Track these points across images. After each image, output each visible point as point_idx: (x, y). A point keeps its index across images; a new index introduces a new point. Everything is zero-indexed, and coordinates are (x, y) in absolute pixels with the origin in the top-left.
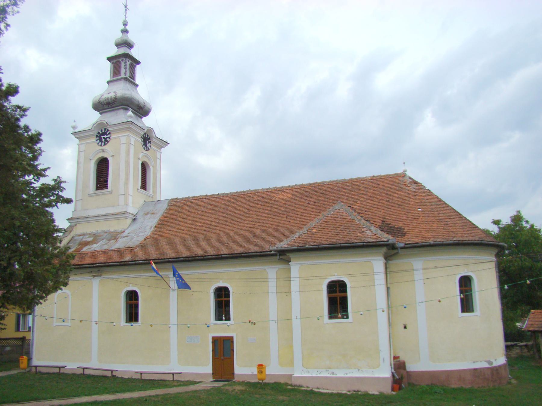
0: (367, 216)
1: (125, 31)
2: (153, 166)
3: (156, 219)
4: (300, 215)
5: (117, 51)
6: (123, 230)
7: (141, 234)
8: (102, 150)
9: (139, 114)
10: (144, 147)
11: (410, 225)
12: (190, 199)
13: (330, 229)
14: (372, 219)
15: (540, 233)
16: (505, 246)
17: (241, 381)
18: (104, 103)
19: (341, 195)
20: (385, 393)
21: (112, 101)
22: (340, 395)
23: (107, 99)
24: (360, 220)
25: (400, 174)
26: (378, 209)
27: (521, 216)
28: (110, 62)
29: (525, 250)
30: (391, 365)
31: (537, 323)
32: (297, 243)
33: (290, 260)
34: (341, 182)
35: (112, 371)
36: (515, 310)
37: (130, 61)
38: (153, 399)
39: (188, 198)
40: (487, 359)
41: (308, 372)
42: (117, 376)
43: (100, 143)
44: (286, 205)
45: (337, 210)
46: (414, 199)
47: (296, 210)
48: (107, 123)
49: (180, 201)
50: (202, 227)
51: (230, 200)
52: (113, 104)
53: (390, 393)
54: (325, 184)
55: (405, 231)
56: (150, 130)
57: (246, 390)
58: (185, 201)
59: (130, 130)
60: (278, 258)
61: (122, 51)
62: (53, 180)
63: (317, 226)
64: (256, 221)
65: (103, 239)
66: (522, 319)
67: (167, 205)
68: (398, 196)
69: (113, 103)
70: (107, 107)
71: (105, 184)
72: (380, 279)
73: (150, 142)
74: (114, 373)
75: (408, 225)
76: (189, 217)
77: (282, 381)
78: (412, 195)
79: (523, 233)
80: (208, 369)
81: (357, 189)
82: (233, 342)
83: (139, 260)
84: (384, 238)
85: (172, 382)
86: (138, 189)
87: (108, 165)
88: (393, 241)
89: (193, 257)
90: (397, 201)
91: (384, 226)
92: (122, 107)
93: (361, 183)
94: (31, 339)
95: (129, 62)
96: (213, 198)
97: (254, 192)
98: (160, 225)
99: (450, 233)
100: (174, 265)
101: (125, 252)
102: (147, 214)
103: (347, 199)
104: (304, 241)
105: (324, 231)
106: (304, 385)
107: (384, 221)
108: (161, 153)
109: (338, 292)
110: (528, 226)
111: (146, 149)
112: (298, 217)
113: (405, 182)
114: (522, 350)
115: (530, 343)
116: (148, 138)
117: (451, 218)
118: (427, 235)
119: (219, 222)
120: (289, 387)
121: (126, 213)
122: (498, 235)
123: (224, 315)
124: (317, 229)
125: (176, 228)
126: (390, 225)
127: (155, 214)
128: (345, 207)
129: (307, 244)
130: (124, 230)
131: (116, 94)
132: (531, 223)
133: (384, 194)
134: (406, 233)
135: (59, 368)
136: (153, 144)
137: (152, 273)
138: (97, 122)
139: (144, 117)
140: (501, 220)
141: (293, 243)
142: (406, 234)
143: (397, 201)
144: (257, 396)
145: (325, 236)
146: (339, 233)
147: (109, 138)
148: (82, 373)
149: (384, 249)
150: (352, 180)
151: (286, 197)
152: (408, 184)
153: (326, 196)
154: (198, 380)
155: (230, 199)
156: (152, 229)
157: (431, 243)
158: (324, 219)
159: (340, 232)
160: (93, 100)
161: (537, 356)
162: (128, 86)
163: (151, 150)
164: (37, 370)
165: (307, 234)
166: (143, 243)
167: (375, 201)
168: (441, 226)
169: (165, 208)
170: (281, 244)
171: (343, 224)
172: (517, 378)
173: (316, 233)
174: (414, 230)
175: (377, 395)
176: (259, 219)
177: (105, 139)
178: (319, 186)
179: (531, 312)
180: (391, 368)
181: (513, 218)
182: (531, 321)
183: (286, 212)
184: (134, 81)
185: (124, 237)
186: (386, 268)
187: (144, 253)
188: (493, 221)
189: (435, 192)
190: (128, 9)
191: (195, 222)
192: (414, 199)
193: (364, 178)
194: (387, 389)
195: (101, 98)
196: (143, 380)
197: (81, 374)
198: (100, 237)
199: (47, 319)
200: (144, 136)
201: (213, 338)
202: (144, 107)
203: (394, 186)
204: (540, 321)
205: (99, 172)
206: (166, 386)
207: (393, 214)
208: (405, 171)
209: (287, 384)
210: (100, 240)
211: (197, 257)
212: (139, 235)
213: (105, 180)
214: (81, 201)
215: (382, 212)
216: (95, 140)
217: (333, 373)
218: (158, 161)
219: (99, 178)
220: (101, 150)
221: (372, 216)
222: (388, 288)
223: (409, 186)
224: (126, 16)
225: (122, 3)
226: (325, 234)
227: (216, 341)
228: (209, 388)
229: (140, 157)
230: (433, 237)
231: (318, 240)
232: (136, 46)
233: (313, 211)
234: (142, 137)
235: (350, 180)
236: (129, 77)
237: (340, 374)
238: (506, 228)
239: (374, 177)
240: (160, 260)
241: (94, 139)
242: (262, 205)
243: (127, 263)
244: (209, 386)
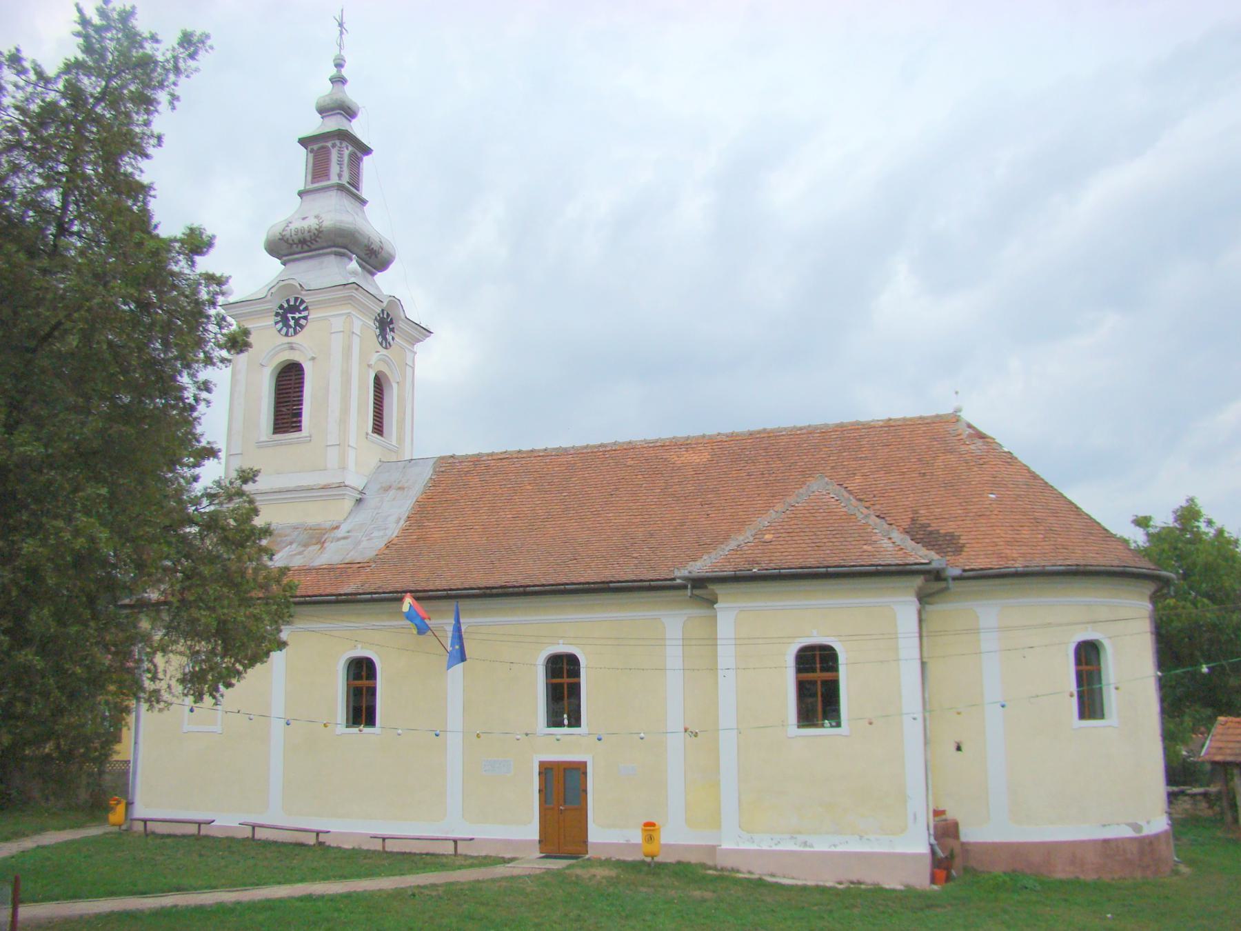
0: (878, 507)
1: (339, 80)
2: (398, 383)
3: (409, 502)
4: (731, 501)
5: (322, 125)
6: (335, 524)
7: (376, 534)
8: (290, 345)
9: (369, 267)
10: (380, 340)
11: (971, 530)
12: (482, 459)
13: (802, 534)
14: (889, 515)
15: (1237, 547)
16: (1173, 579)
17: (603, 858)
19: (820, 459)
20: (918, 887)
21: (311, 237)
22: (822, 890)
24: (867, 516)
25: (948, 415)
26: (903, 493)
27: (1197, 509)
29: (1204, 585)
30: (928, 829)
31: (1231, 745)
32: (733, 564)
33: (717, 599)
34: (818, 431)
35: (318, 833)
36: (1178, 717)
37: (350, 148)
38: (426, 892)
39: (478, 455)
40: (1130, 821)
41: (752, 840)
42: (327, 844)
43: (285, 330)
44: (700, 478)
45: (817, 493)
46: (980, 472)
47: (721, 489)
48: (301, 286)
49: (462, 462)
50: (514, 522)
51: (574, 463)
52: (312, 243)
53: (928, 889)
54: (784, 433)
55: (961, 541)
56: (395, 302)
57: (618, 877)
58: (472, 463)
59: (352, 303)
60: (689, 594)
61: (333, 124)
63: (773, 528)
64: (634, 511)
65: (291, 543)
66: (1194, 736)
67: (431, 472)
68: (945, 465)
69: (313, 242)
70: (299, 249)
71: (295, 420)
72: (909, 647)
73: (392, 330)
74: (322, 838)
75: (969, 530)
76: (483, 499)
77: (693, 858)
78: (974, 463)
79: (1201, 547)
80: (532, 832)
81: (855, 447)
82: (585, 773)
83: (381, 591)
84: (921, 557)
85: (453, 857)
86: (367, 434)
87: (303, 378)
88: (940, 564)
89: (501, 587)
90: (941, 476)
91: (916, 529)
92: (334, 249)
93: (864, 434)
94: (132, 759)
95: (347, 149)
96: (535, 457)
97: (625, 447)
99: (1057, 548)
100: (460, 603)
101: (346, 572)
102: (388, 489)
103: (833, 468)
104: (748, 559)
105: (789, 538)
106: (744, 869)
107: (916, 519)
109: (818, 670)
110: (1212, 532)
112: (728, 504)
113: (958, 435)
114: (1196, 804)
115: (1213, 789)
116: (389, 320)
117: (1060, 515)
118: (1008, 551)
119: (552, 510)
120: (711, 872)
121: (343, 485)
122: (1146, 549)
123: (565, 716)
124: (773, 534)
125: (454, 522)
126: (929, 529)
127: (406, 489)
128: (834, 488)
129: (755, 565)
130: (338, 525)
131: (321, 221)
132: (1218, 523)
133: (915, 460)
134: (963, 546)
135: (197, 825)
138: (278, 283)
139: (379, 273)
140: (1153, 516)
141: (725, 564)
142: (966, 549)
143: (941, 476)
144: (644, 890)
145: (792, 549)
146: (823, 544)
147: (305, 318)
148: (250, 835)
149: (919, 581)
150: (842, 427)
151: (698, 460)
152: (966, 438)
153: (787, 461)
154: (508, 855)
155: (573, 462)
156: (402, 522)
157: (1019, 569)
158: (788, 512)
159: (825, 540)
161: (1229, 817)
162: (348, 203)
164: (148, 828)
165: (753, 544)
166: (384, 554)
167: (893, 474)
168: (1039, 532)
169: (428, 478)
170: (699, 564)
171: (830, 525)
172: (1191, 862)
173: (772, 543)
174: (980, 541)
175: (901, 891)
176: (640, 507)
177: (297, 321)
178: (769, 437)
179: (1217, 722)
180: (929, 834)
181: (1179, 513)
182: (1219, 741)
183: (699, 494)
184: (357, 192)
185: (339, 539)
186: (920, 621)
187: (389, 577)
188: (1135, 518)
189: (1023, 458)
190: (346, 30)
191: (498, 511)
192: (980, 472)
193: (868, 423)
194: (921, 879)
195: (287, 228)
196: (387, 852)
197: (248, 838)
198: (285, 538)
199: (251, 719)
200: (381, 315)
201: (542, 764)
202: (380, 250)
203: (935, 443)
204: (1238, 742)
205: (279, 394)
206: (444, 866)
207: (934, 503)
208: (958, 410)
209: (704, 866)
210: (284, 545)
211: (510, 587)
212: (372, 535)
213: (294, 411)
214: (240, 456)
215: (910, 499)
216: (273, 323)
217: (805, 844)
218: (409, 370)
219: (280, 407)
220: (286, 346)
221: (888, 508)
222: (923, 664)
223: (967, 443)
224: (340, 46)
225: (334, 17)
226: (794, 546)
227: (547, 770)
228: (538, 872)
229: (372, 362)
230: (1022, 555)
231: (778, 558)
232: (362, 113)
233: (759, 492)
234: (376, 319)
235: (837, 425)
236: (348, 182)
237: (821, 845)
238: (1163, 536)
239: (891, 422)
240: (426, 593)
241: (271, 320)
242: (646, 476)
243: (353, 597)
244: (537, 867)
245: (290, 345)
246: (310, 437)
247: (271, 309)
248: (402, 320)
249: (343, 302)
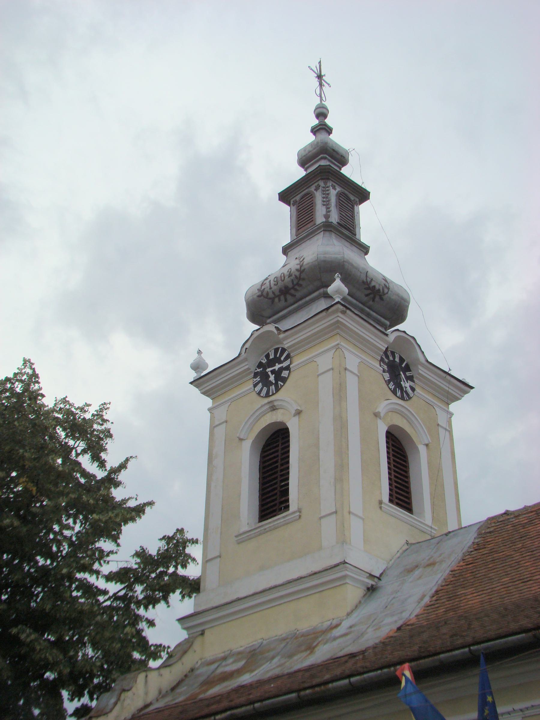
2: (427, 445)
6: (335, 622)
10: (392, 386)
18: (273, 293)
21: (292, 281)
23: (279, 279)
28: (289, 205)
37: (338, 189)
52: (296, 290)
58: (534, 513)
62: (164, 538)
69: (297, 287)
71: (283, 499)
86: (381, 502)
98: (450, 586)
108: (451, 414)
111: (399, 394)
136: (420, 383)
147: (288, 368)
163: (414, 399)
177: (277, 374)
198: (267, 654)
202: (386, 291)
224: (321, 96)
234: (382, 360)
245: (271, 405)
246: (300, 512)
247: (248, 369)
248: (422, 365)
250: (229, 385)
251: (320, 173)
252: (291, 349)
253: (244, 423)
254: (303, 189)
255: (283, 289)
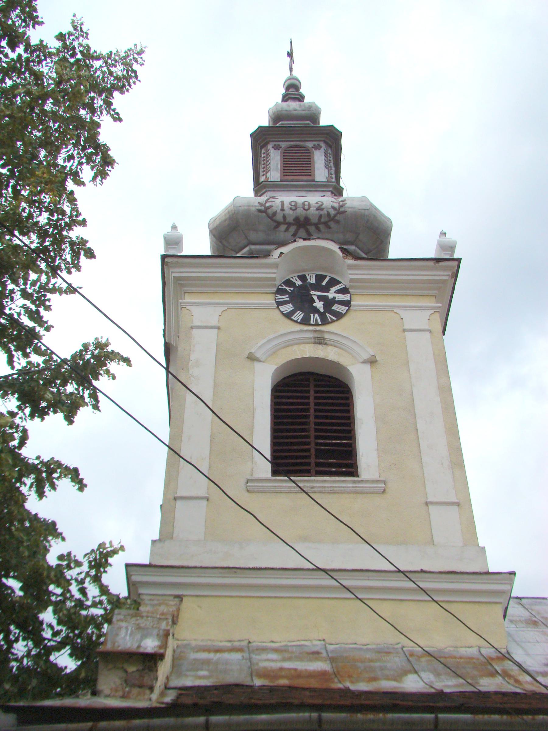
8: (316, 335)
18: (284, 217)
21: (320, 216)
69: (321, 227)
137: (223, 646)
160: (209, 225)
245: (316, 335)
247: (274, 279)
249: (425, 292)
250: (226, 286)
251: (327, 134)
252: (357, 284)
253: (265, 341)
254: (293, 139)
255: (302, 219)
